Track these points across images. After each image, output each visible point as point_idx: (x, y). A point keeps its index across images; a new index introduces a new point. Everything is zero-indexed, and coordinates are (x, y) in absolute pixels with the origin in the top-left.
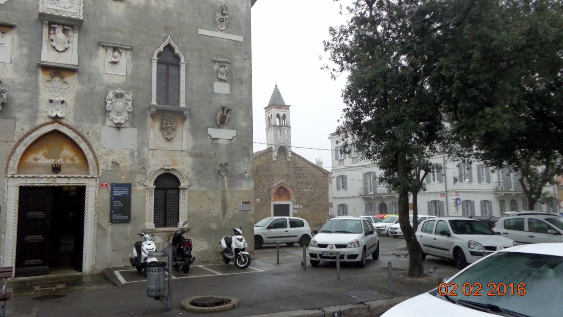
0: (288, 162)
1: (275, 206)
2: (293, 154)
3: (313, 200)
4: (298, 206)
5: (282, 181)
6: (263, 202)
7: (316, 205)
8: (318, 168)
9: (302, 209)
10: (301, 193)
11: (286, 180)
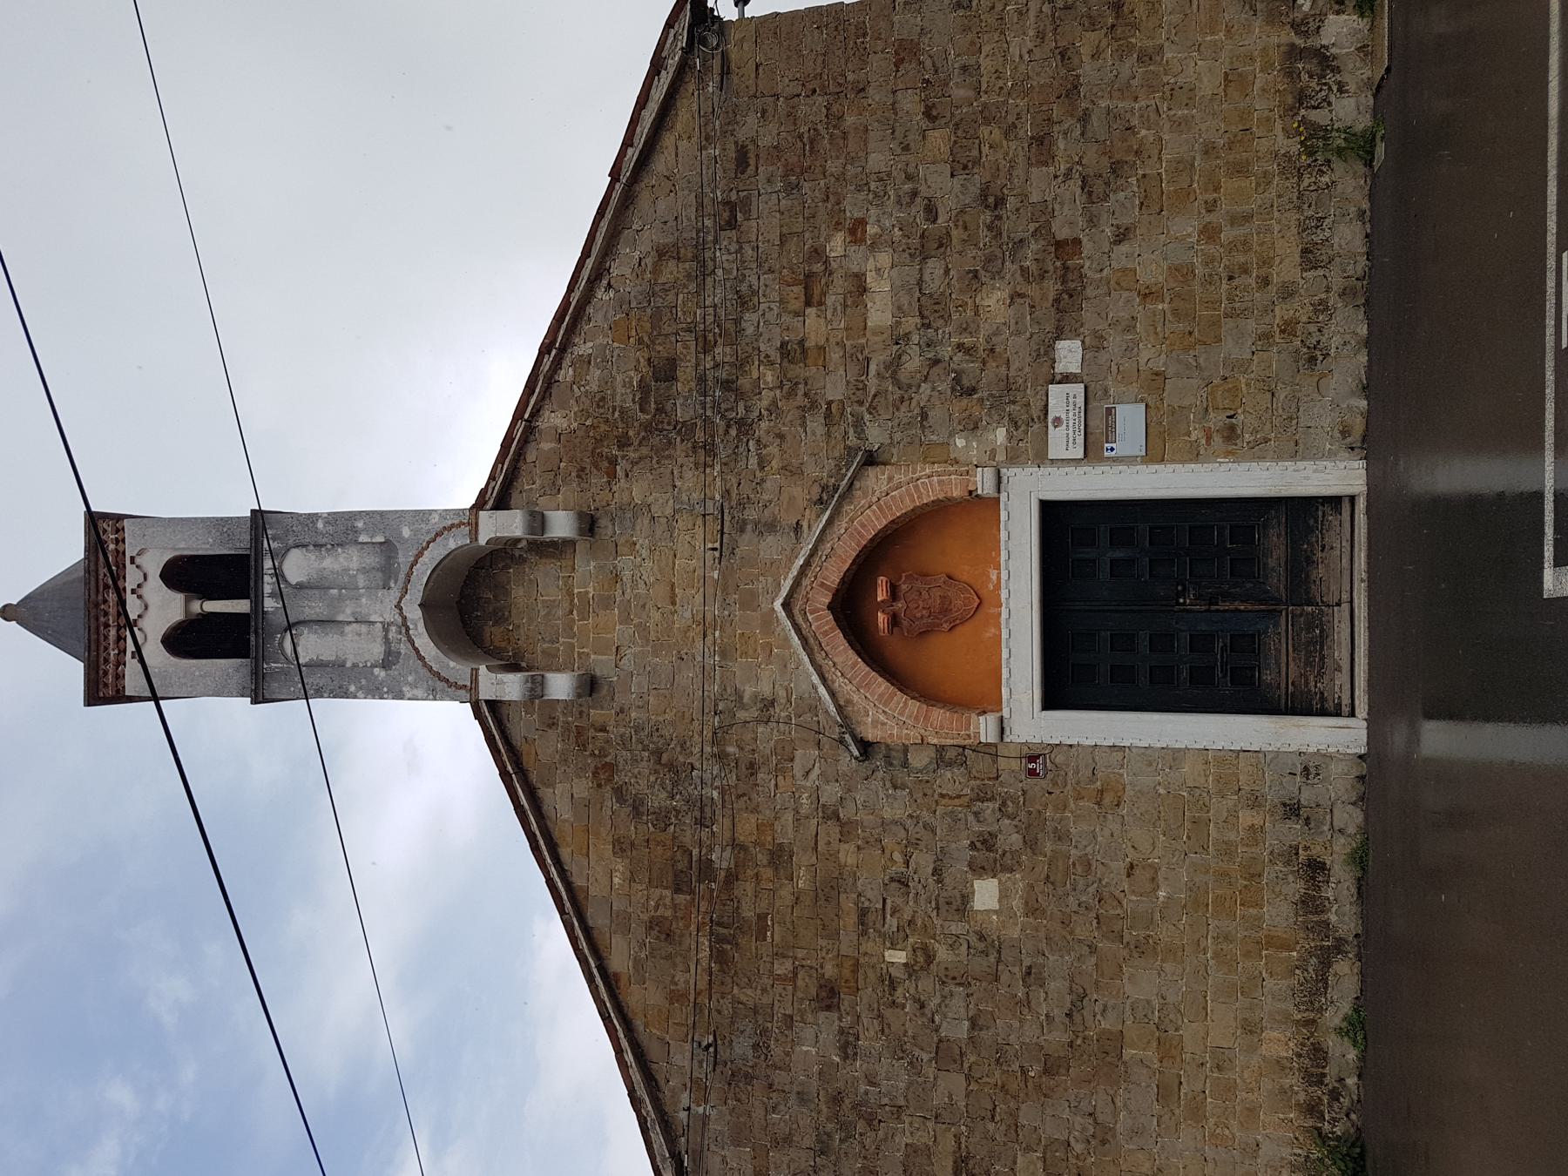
0: (589, 525)
1: (1053, 699)
2: (498, 494)
3: (992, 200)
4: (1063, 401)
5: (778, 605)
6: (1011, 839)
9: (1094, 346)
10: (913, 363)
11: (771, 546)
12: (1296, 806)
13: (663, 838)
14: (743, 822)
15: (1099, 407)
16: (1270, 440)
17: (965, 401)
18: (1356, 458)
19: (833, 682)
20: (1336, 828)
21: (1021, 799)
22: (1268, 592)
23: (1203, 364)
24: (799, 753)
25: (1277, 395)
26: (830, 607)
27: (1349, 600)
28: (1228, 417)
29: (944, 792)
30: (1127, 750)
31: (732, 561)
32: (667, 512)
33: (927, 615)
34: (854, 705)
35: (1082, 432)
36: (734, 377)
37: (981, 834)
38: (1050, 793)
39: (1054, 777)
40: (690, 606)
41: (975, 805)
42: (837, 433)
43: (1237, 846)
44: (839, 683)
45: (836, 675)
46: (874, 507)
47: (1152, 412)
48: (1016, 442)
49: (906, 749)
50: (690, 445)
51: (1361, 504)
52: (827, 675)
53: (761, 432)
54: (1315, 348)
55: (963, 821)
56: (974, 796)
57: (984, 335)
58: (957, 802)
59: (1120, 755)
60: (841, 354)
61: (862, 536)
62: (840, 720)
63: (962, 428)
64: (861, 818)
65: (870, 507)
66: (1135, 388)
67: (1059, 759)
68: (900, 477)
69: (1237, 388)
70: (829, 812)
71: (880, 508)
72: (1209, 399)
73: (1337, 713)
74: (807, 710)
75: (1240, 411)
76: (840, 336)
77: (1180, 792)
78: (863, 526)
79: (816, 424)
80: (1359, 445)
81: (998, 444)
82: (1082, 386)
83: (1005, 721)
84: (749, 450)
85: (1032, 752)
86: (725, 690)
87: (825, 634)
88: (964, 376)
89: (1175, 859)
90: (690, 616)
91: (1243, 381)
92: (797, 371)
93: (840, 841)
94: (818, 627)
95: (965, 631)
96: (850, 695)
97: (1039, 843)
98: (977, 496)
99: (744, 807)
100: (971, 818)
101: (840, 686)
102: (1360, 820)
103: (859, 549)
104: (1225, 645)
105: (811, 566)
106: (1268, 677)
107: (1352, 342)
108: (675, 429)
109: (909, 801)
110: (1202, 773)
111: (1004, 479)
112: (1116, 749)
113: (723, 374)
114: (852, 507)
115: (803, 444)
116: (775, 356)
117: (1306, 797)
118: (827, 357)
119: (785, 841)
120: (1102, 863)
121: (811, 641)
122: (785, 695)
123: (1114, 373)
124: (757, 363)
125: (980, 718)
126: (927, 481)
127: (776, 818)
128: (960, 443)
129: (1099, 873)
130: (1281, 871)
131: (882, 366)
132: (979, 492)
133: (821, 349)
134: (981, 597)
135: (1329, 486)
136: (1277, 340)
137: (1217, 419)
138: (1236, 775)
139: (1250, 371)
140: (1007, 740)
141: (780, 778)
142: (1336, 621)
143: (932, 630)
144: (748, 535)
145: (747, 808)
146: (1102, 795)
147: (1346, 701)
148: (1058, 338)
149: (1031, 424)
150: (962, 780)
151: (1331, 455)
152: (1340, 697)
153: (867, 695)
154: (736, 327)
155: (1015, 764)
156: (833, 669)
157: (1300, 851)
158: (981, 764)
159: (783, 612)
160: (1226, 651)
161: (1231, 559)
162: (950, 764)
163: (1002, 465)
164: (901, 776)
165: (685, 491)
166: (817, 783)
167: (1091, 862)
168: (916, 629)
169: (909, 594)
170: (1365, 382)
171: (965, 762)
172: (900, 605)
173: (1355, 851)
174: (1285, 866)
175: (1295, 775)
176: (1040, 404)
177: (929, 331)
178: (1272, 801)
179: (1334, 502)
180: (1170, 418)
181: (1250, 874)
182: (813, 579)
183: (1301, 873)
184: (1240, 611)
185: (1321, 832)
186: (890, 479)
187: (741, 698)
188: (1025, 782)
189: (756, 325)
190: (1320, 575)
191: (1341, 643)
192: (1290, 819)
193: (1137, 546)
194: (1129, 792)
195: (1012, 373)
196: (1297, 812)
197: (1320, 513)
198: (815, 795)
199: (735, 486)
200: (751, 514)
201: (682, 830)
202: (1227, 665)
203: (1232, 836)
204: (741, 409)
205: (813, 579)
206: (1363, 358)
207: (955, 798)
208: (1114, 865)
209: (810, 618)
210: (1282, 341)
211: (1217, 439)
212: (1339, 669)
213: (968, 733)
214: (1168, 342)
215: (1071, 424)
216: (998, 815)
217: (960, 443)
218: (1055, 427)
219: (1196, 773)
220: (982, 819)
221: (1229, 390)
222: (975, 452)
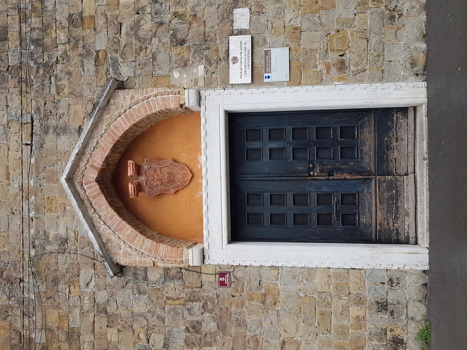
5: (63, 179)
12: (385, 304)
13: (4, 324)
14: (50, 314)
15: (260, 51)
16: (366, 70)
17: (179, 49)
18: (420, 81)
19: (99, 228)
20: (410, 317)
21: (216, 301)
22: (363, 167)
23: (324, 22)
24: (82, 272)
25: (370, 41)
26: (97, 180)
27: (413, 172)
28: (340, 56)
29: (170, 296)
30: (280, 268)
31: (41, 152)
32: (4, 122)
33: (160, 184)
34: (112, 242)
35: (250, 66)
36: (41, 37)
37: (192, 322)
38: (233, 296)
39: (236, 285)
40: (18, 181)
41: (188, 304)
42: (103, 70)
43: (349, 329)
44: (102, 228)
45: (101, 224)
46: (123, 116)
47: (293, 53)
48: (210, 74)
49: (146, 269)
50: (16, 80)
51: (423, 111)
52: (95, 224)
53: (58, 71)
54: (394, 10)
55: (181, 314)
56: (187, 298)
57: (190, 6)
58: (177, 302)
59: (275, 272)
60: (104, 21)
61: (116, 135)
62: (101, 253)
63: (177, 65)
64: (120, 313)
65: (120, 116)
66: (282, 38)
67: (239, 275)
68: (138, 97)
69: (345, 37)
70: (100, 309)
71: (126, 116)
72: (328, 44)
73: (406, 241)
74: (86, 245)
75: (347, 52)
76: (103, 10)
77: (313, 295)
78: (116, 128)
79: (90, 65)
80: (421, 72)
81: (199, 75)
82: (250, 36)
83: (205, 251)
84: (51, 83)
85: (222, 270)
86: (39, 232)
87: (94, 197)
88: (178, 33)
89: (311, 337)
90: (18, 187)
91: (349, 32)
92: (78, 32)
93: (108, 326)
94: (90, 193)
95: (184, 193)
96: (109, 236)
97: (227, 329)
98: (186, 108)
99: (51, 305)
100: (186, 312)
101: (103, 230)
102: (425, 311)
103: (113, 143)
104: (338, 200)
105: (85, 154)
106: (364, 220)
107: (417, 6)
108: (8, 70)
109: (148, 301)
110: (326, 283)
111: (203, 98)
112: (273, 268)
113: (35, 35)
114: (109, 116)
115: (82, 78)
116: (65, 23)
117: (391, 297)
118: (96, 24)
119: (76, 326)
120: (266, 341)
121: (86, 202)
122: (74, 236)
123: (270, 29)
124: (54, 28)
125: (189, 250)
126: (154, 98)
127: (70, 312)
128: (176, 75)
129: (264, 347)
130: (376, 345)
131: (129, 28)
132: (187, 105)
133: (92, 18)
134: (194, 172)
135: (403, 98)
136: (370, 6)
137: (333, 57)
138: (347, 284)
139: (353, 26)
140: (207, 262)
141: (72, 287)
142: (405, 184)
143: (164, 194)
144: (51, 136)
145: (53, 306)
146: (265, 297)
147: (412, 235)
148: (235, 7)
149: (219, 63)
150: (180, 288)
151: (405, 79)
152: (408, 232)
153: (120, 236)
154: (42, 6)
155: (212, 278)
156: (99, 220)
157: (388, 332)
158: (191, 278)
159: (66, 184)
160: (339, 204)
161: (341, 147)
162: (173, 278)
163: (202, 88)
164: (143, 286)
165: (14, 109)
166: (94, 290)
167: (259, 340)
168: (154, 192)
169: (148, 171)
170: (425, 32)
171: (182, 277)
172: (142, 178)
173: (422, 332)
174: (379, 342)
175: (384, 283)
176: (225, 49)
177: (157, 4)
178: (370, 300)
179: (404, 110)
180: (305, 57)
181: (357, 347)
182: (86, 162)
183: (388, 346)
184: (347, 179)
185: (401, 320)
186: (132, 98)
187: (48, 237)
188: (218, 289)
189: (53, 3)
190: (395, 157)
191: (408, 199)
192: (381, 312)
193: (285, 140)
194: (282, 296)
195: (207, 30)
196: (385, 307)
197: (395, 118)
198: (92, 298)
199: (43, 104)
200: (52, 122)
201: (15, 319)
202: (339, 213)
203: (346, 323)
204: (46, 58)
205: (86, 162)
206: (423, 17)
207: (176, 300)
208: (273, 342)
209: (85, 187)
210: (374, 6)
211: (334, 70)
212: (407, 214)
213: (181, 259)
214: (302, 8)
215: (243, 61)
216: (202, 310)
217: (176, 75)
218: (234, 63)
219: (323, 283)
220: (192, 313)
221: (340, 39)
222: (185, 81)
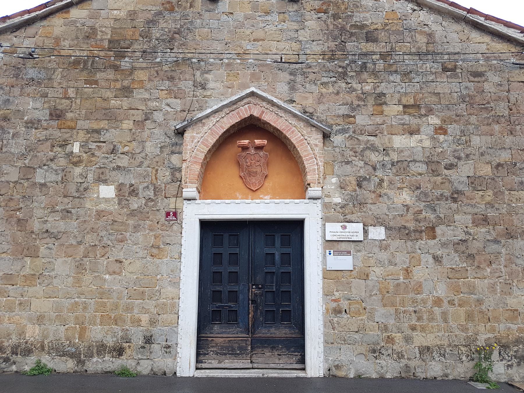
6: (135, 204)
7: (476, 223)
8: (481, 20)
9: (382, 246)
10: (374, 157)
